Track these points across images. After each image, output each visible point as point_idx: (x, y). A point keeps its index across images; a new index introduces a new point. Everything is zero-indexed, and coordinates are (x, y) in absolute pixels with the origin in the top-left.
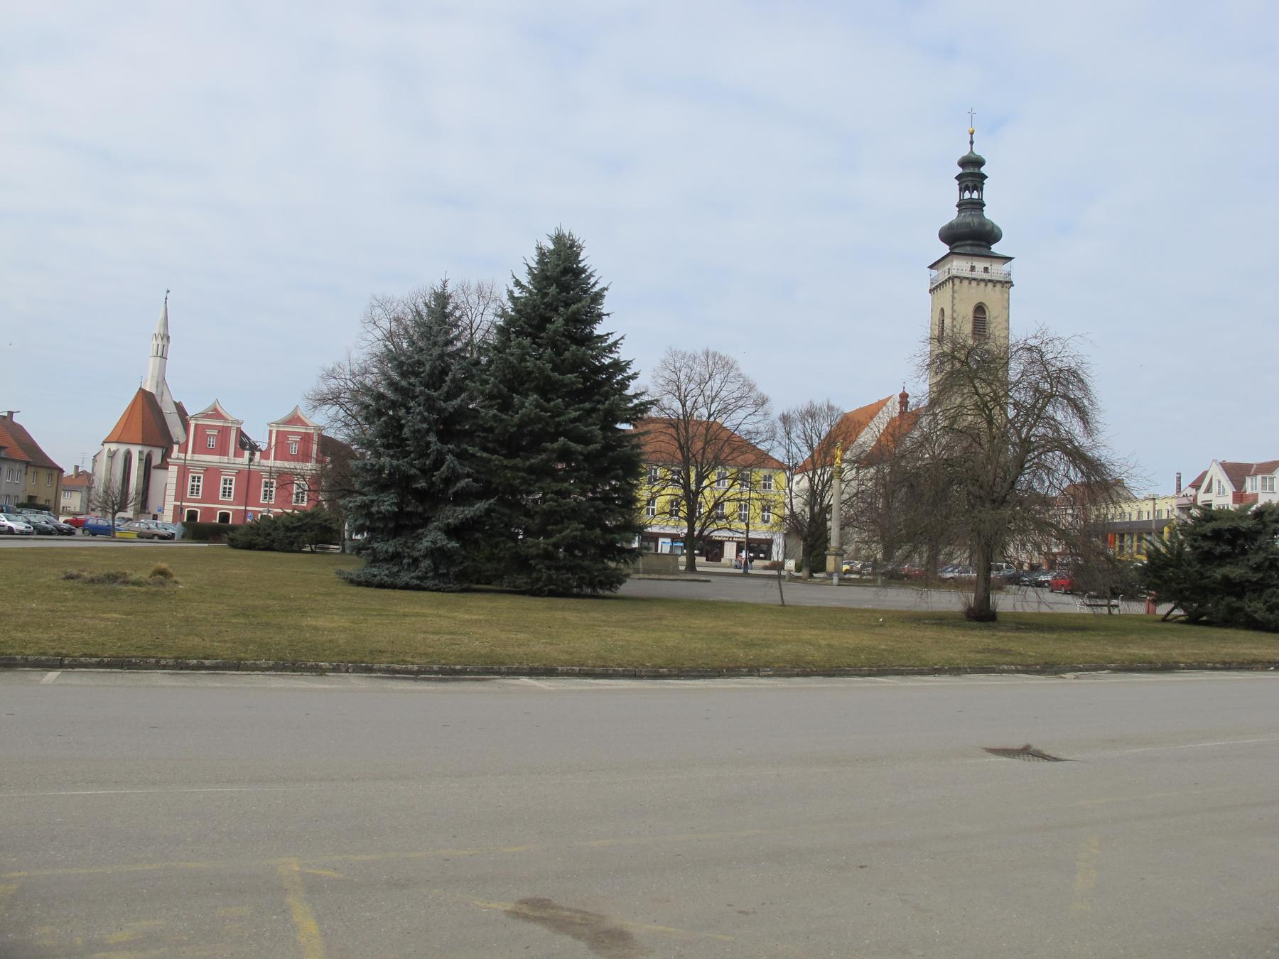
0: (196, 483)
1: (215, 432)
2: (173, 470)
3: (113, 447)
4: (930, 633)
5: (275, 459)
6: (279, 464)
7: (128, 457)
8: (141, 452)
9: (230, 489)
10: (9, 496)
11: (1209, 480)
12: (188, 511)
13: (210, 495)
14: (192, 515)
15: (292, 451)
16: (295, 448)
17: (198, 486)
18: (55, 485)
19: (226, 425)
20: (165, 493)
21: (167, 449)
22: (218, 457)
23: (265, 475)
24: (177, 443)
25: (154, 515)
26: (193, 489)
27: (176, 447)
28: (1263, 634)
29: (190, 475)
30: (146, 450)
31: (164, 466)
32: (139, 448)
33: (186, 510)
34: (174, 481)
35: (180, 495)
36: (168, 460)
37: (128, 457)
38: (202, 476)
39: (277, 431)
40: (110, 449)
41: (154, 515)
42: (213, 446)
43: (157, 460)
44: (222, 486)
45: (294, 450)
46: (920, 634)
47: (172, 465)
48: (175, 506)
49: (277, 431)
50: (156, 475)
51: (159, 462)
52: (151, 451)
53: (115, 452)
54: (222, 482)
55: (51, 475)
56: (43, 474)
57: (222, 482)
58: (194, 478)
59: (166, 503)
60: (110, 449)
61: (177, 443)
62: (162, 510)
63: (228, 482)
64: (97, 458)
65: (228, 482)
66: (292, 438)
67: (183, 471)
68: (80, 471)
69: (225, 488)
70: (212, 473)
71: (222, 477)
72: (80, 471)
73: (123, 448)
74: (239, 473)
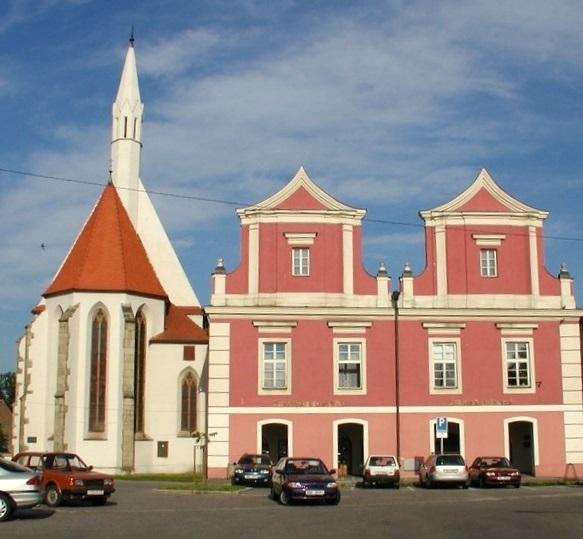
0: (275, 361)
1: (350, 228)
5: (451, 290)
6: (458, 300)
7: (100, 320)
8: (126, 309)
11: (503, 202)
13: (311, 384)
14: (275, 436)
15: (297, 269)
16: (305, 260)
17: (523, 366)
22: (322, 294)
28: (180, 413)
32: (123, 299)
33: (507, 422)
37: (100, 320)
47: (216, 321)
48: (232, 417)
51: (160, 329)
59: (210, 410)
66: (294, 240)
70: (311, 338)
71: (336, 340)
74: (373, 330)
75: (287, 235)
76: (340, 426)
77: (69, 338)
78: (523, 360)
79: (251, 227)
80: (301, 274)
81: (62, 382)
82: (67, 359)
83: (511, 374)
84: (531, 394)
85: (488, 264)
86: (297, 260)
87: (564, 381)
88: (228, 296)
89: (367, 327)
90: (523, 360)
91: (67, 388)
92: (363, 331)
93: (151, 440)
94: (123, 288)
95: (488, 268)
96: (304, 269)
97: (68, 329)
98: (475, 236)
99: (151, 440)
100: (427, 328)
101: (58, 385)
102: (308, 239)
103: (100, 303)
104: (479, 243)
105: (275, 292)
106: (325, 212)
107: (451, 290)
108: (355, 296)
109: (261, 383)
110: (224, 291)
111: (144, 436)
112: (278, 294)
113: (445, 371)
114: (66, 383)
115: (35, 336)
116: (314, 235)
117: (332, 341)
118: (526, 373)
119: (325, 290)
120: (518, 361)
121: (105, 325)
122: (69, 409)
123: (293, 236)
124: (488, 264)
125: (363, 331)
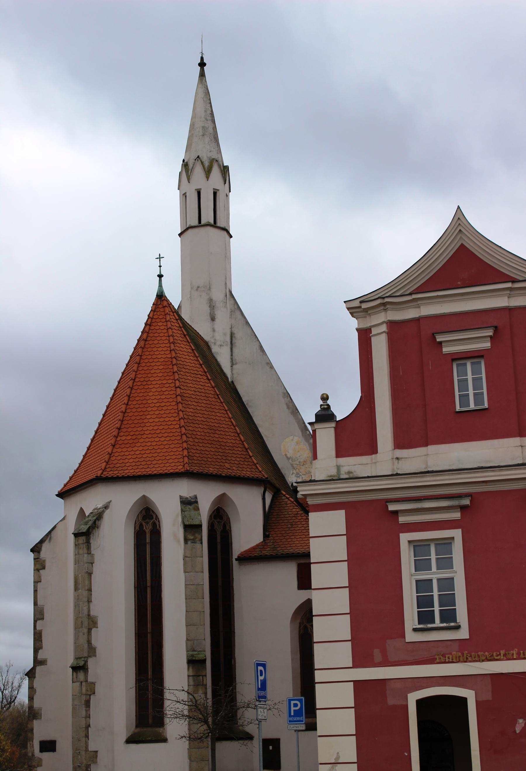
7: (148, 528)
15: (464, 398)
16: (477, 381)
29: (404, 538)
33: (413, 698)
37: (148, 528)
38: (457, 534)
49: (392, 325)
71: (404, 538)
75: (435, 335)
76: (464, 701)
78: (445, 574)
79: (374, 331)
81: (83, 640)
82: (89, 601)
86: (463, 383)
88: (399, 453)
89: (463, 508)
90: (423, 576)
91: (92, 651)
92: (457, 515)
94: (180, 469)
95: (471, 392)
96: (478, 397)
98: (439, 338)
99: (250, 737)
100: (396, 513)
101: (77, 647)
103: (144, 498)
104: (446, 350)
105: (426, 445)
106: (509, 285)
110: (333, 453)
111: (190, 731)
112: (432, 448)
113: (436, 593)
114: (89, 642)
115: (47, 565)
121: (156, 533)
122: (98, 689)
125: (457, 515)
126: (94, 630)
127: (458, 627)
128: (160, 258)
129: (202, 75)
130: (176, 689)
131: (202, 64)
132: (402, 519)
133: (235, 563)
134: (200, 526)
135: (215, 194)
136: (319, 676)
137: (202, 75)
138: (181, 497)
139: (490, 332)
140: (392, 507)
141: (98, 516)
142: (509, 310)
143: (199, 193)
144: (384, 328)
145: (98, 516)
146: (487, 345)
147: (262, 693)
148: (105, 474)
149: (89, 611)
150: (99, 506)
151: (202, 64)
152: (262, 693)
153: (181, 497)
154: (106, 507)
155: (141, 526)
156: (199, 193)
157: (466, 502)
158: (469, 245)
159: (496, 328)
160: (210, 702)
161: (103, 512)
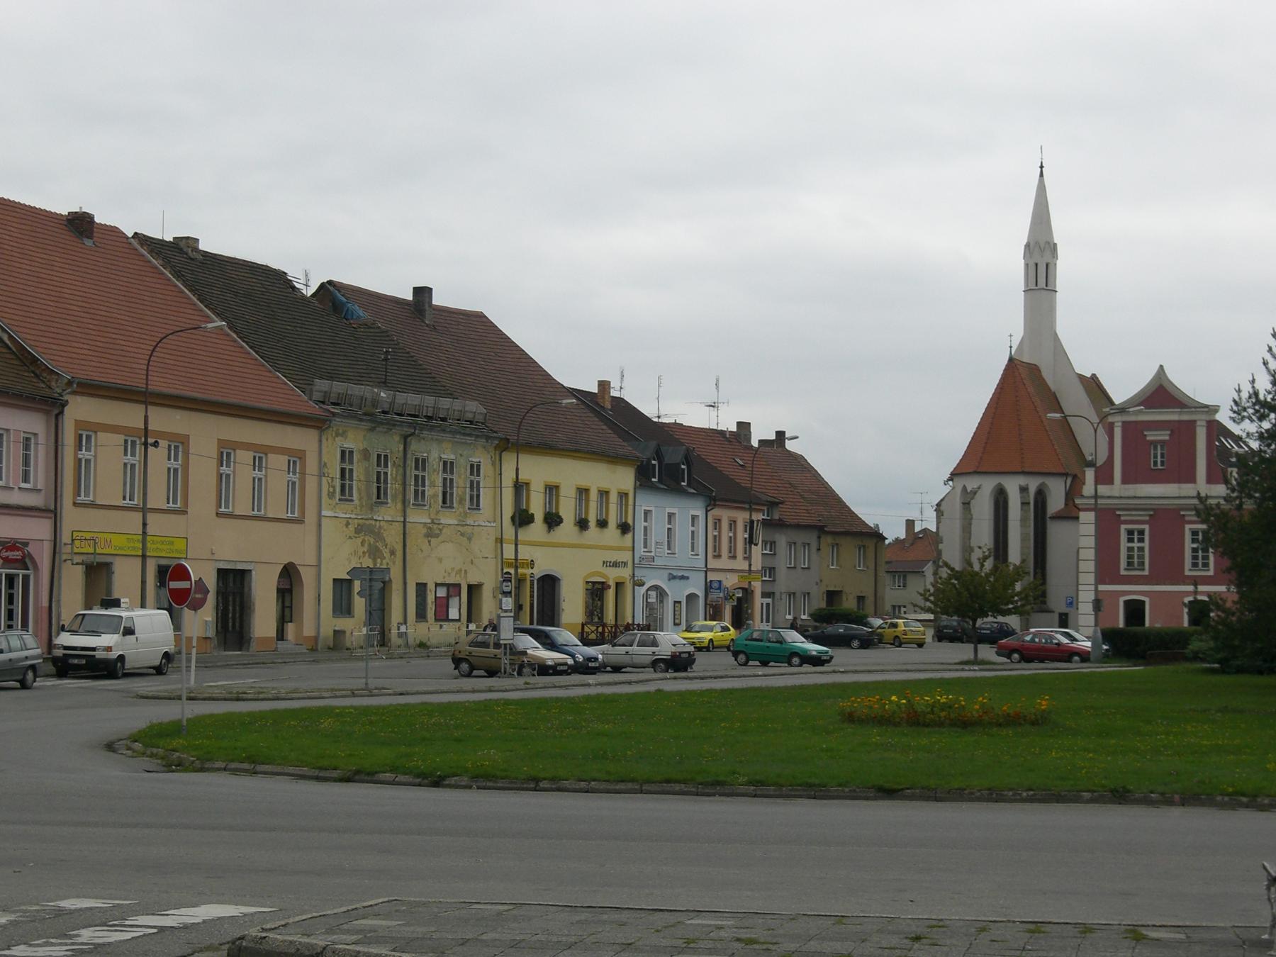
0: (1136, 545)
2: (1087, 518)
3: (972, 483)
4: (875, 735)
5: (1125, 481)
8: (1024, 490)
9: (1141, 549)
10: (794, 593)
12: (1126, 602)
14: (1135, 611)
18: (872, 566)
19: (1185, 417)
20: (1078, 567)
21: (1075, 477)
22: (1176, 485)
23: (1191, 516)
24: (1091, 464)
25: (1061, 615)
26: (1139, 557)
27: (1090, 474)
29: (1123, 527)
30: (1033, 484)
31: (1070, 514)
33: (1122, 599)
34: (1091, 542)
35: (1106, 570)
36: (1078, 501)
38: (1146, 527)
39: (1124, 423)
40: (964, 488)
41: (1061, 615)
42: (1162, 463)
43: (1056, 502)
44: (1124, 545)
45: (1157, 459)
46: (925, 741)
49: (1124, 423)
50: (1056, 532)
52: (1043, 484)
53: (975, 493)
54: (1124, 537)
55: (862, 548)
56: (849, 549)
57: (1124, 537)
58: (1130, 532)
60: (964, 488)
61: (1091, 464)
62: (1072, 603)
63: (1136, 537)
64: (942, 508)
65: (1136, 537)
67: (1108, 520)
68: (917, 529)
69: (1131, 549)
71: (1123, 527)
72: (917, 529)
73: (987, 485)
76: (1144, 602)
77: (971, 519)
78: (1130, 545)
80: (1160, 467)
82: (970, 539)
83: (1130, 557)
84: (1210, 576)
85: (1159, 457)
86: (1155, 457)
87: (1093, 569)
89: (1150, 515)
92: (1147, 518)
93: (1053, 612)
97: (970, 510)
98: (1145, 433)
99: (1053, 612)
100: (1119, 515)
102: (1164, 436)
104: (1148, 438)
107: (1125, 481)
108: (1208, 485)
109: (1123, 564)
116: (1169, 432)
117: (1184, 527)
118: (1128, 558)
119: (1179, 481)
120: (1136, 545)
123: (1151, 433)
124: (1159, 457)
125: (1147, 518)
126: (972, 554)
127: (1143, 570)
128: (1011, 336)
129: (1042, 175)
130: (657, 401)
131: (1042, 167)
132: (1122, 518)
133: (1048, 519)
134: (1029, 503)
135: (1047, 265)
136: (1081, 587)
137: (1042, 175)
138: (1020, 485)
139: (1169, 432)
140: (1118, 513)
141: (974, 493)
142: (1179, 422)
143: (1037, 265)
144: (1120, 424)
145: (974, 493)
146: (1167, 438)
147: (10, 623)
148: (979, 470)
149: (970, 543)
150: (975, 487)
151: (1042, 167)
152: (10, 623)
153: (1020, 485)
154: (979, 488)
155: (997, 498)
156: (1037, 265)
157: (1152, 513)
158: (1165, 384)
159: (1172, 431)
160: (370, 424)
161: (977, 491)
